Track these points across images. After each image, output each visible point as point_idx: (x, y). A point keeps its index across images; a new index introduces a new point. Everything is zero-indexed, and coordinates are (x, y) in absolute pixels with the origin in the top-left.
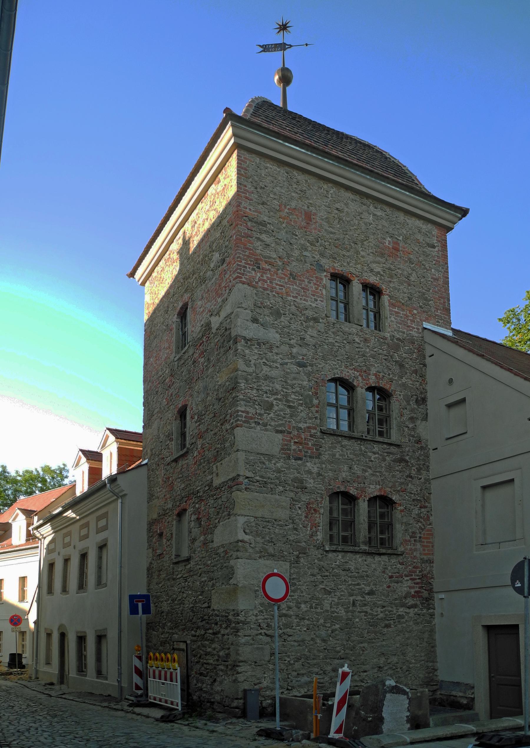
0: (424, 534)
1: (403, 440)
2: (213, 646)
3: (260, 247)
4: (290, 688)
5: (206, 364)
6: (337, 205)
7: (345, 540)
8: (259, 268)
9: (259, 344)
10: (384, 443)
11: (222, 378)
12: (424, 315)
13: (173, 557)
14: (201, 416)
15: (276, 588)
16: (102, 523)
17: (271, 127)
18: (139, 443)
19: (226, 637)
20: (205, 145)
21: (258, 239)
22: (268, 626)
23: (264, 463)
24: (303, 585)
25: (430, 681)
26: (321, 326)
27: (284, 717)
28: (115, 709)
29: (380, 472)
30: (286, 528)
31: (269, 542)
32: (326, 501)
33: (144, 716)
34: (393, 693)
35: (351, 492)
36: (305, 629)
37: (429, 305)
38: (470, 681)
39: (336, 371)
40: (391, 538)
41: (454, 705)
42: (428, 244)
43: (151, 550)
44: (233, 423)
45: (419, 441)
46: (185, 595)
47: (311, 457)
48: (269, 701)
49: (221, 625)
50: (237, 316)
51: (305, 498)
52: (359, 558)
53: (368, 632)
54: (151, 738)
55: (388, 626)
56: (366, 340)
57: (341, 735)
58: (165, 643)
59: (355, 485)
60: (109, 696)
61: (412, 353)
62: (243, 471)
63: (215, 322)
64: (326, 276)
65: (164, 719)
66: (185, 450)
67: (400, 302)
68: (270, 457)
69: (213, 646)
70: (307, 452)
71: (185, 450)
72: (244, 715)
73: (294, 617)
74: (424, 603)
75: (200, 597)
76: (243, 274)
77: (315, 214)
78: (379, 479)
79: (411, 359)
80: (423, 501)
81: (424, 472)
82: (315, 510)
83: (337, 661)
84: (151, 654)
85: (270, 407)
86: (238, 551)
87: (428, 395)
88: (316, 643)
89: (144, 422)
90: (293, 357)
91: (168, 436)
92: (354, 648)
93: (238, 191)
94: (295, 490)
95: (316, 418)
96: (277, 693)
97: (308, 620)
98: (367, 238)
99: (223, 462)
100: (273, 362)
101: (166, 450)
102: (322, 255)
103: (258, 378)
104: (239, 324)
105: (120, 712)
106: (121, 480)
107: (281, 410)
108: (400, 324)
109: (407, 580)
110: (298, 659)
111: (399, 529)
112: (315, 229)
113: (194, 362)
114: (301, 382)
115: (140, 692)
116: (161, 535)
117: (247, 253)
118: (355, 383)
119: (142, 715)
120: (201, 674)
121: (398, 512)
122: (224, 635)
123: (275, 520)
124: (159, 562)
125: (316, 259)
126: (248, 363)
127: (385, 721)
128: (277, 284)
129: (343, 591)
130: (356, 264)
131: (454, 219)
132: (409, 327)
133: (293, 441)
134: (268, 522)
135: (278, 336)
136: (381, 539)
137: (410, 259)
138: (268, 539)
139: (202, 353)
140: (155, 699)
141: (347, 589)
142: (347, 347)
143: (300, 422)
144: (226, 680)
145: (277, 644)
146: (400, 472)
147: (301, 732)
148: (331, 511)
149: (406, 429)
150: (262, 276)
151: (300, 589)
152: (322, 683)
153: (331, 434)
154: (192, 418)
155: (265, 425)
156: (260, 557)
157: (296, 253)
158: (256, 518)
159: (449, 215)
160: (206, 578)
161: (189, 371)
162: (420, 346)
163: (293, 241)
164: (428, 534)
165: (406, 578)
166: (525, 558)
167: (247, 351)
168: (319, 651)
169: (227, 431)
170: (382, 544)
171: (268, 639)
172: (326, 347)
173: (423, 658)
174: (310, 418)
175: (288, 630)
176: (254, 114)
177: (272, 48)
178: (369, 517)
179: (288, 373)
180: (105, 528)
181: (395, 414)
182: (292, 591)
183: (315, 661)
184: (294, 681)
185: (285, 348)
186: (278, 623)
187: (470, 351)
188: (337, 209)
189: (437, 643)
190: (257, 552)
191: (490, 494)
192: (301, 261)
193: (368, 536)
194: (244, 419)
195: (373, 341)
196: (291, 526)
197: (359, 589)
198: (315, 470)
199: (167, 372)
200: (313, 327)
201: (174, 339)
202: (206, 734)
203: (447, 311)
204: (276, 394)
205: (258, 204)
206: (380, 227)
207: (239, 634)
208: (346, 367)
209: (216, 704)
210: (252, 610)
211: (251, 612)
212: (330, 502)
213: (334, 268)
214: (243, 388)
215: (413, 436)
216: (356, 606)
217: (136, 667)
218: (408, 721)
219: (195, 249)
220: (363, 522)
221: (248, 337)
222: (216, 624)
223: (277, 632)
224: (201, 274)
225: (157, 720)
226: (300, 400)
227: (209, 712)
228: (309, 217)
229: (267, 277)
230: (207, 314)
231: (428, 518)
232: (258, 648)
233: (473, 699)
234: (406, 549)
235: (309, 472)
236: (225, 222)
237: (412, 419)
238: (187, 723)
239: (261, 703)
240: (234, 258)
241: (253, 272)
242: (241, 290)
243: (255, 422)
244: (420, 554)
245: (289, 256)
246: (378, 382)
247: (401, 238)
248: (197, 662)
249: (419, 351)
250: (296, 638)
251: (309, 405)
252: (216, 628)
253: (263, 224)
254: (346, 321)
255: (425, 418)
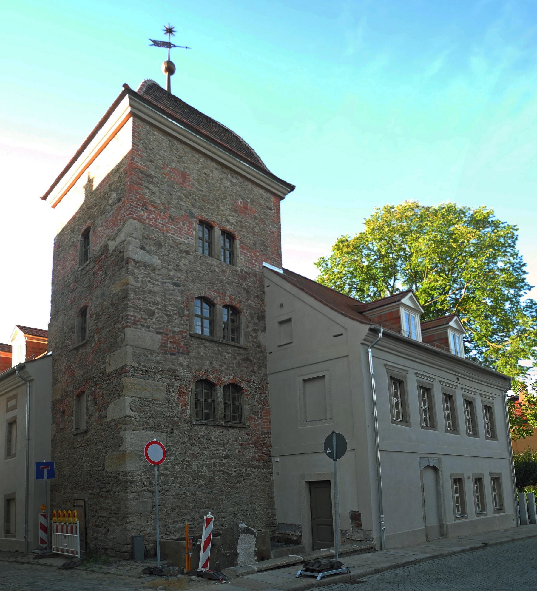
0: (264, 413)
1: (248, 345)
2: (107, 502)
3: (148, 194)
4: (168, 533)
5: (103, 276)
6: (205, 171)
7: (207, 416)
8: (146, 209)
9: (145, 266)
10: (235, 346)
11: (116, 289)
12: (264, 257)
13: (74, 430)
14: (98, 316)
15: (156, 453)
16: (12, 403)
17: (159, 105)
18: (45, 339)
19: (117, 493)
20: (107, 108)
21: (147, 187)
22: (151, 483)
23: (147, 356)
24: (176, 451)
25: (271, 524)
26: (191, 258)
27: (164, 557)
28: (21, 563)
29: (232, 367)
30: (163, 406)
31: (150, 417)
32: (193, 387)
33: (48, 566)
34: (245, 533)
35: (211, 380)
36: (179, 485)
37: (267, 250)
38: (298, 523)
39: (201, 291)
40: (241, 415)
41: (288, 541)
42: (267, 207)
43: (55, 425)
44: (123, 324)
45: (259, 346)
46: (83, 461)
47: (182, 354)
48: (152, 545)
49: (113, 484)
50: (129, 243)
51: (177, 384)
52: (218, 430)
53: (225, 487)
54: (54, 584)
55: (239, 482)
56: (223, 271)
57: (207, 568)
58: (66, 502)
59: (214, 375)
60: (17, 551)
61: (255, 283)
62: (130, 362)
63: (112, 245)
64: (195, 221)
65: (66, 567)
66: (85, 341)
67: (248, 246)
68: (152, 352)
69: (107, 502)
70: (179, 350)
71: (85, 341)
72: (132, 557)
73: (170, 476)
74: (265, 465)
75: (96, 462)
76: (134, 212)
77: (189, 175)
78: (231, 372)
79: (254, 287)
80: (263, 388)
81: (263, 369)
82: (184, 393)
83: (203, 510)
84: (55, 512)
85: (152, 314)
86: (126, 424)
87: (266, 314)
88: (187, 496)
89: (51, 316)
90: (170, 278)
91: (71, 329)
92: (215, 499)
93: (132, 149)
94: (170, 377)
95: (187, 325)
96: (158, 538)
97: (181, 478)
98: (225, 197)
99: (115, 353)
100: (156, 280)
101: (69, 340)
102: (193, 205)
103: (143, 291)
104: (130, 249)
105: (25, 565)
106: (28, 368)
107: (161, 317)
108: (247, 262)
109: (252, 447)
110: (173, 510)
111: (246, 408)
112: (189, 186)
113: (94, 274)
114: (176, 298)
115: (44, 545)
116: (63, 412)
117: (138, 197)
118: (215, 302)
119: (46, 565)
120: (97, 526)
121: (245, 396)
122: (115, 492)
123: (155, 400)
124: (62, 434)
125: (189, 208)
126: (136, 279)
127: (239, 555)
128: (160, 223)
129: (206, 455)
130: (217, 215)
131: (285, 192)
132: (253, 264)
133: (169, 341)
134: (149, 401)
135: (159, 261)
136: (234, 416)
137: (255, 216)
138: (149, 414)
139: (101, 267)
140: (58, 550)
141: (209, 454)
142: (210, 275)
143: (175, 327)
144: (117, 529)
145: (157, 498)
146: (247, 368)
147: (177, 568)
148: (197, 395)
149: (251, 337)
150: (149, 215)
151: (174, 454)
152: (192, 528)
153: (197, 338)
154: (91, 316)
155: (148, 327)
156: (143, 429)
157: (175, 202)
158: (140, 398)
159: (282, 188)
160: (100, 447)
161: (90, 280)
162: (261, 278)
163: (172, 192)
164: (266, 413)
165: (252, 446)
166: (333, 432)
167: (136, 271)
168: (189, 502)
169: (119, 329)
170: (234, 420)
171: (150, 494)
172: (194, 273)
173: (265, 506)
174: (182, 325)
175: (166, 486)
176: (146, 92)
177: (161, 44)
178: (225, 399)
179: (166, 290)
180: (15, 407)
181: (243, 326)
182: (168, 456)
183: (187, 511)
184: (171, 528)
185: (164, 271)
186: (158, 481)
187: (295, 285)
188: (205, 174)
189: (275, 495)
190: (141, 425)
191: (309, 386)
192: (178, 208)
193: (224, 414)
194: (132, 322)
195: (228, 272)
196: (167, 405)
197: (218, 454)
198: (185, 363)
199: (72, 278)
200: (185, 258)
201: (78, 254)
202: (101, 576)
203: (280, 255)
204: (157, 304)
205: (147, 161)
206: (235, 191)
207: (127, 491)
208: (209, 289)
209: (109, 550)
210: (137, 471)
211: (137, 473)
212: (196, 388)
213: (202, 216)
214: (132, 298)
215: (256, 343)
216: (216, 467)
217: (41, 524)
218: (255, 555)
219: (98, 187)
220: (222, 403)
221: (137, 260)
222: (109, 483)
223: (157, 488)
224: (102, 207)
225: (59, 568)
226: (175, 310)
227: (104, 558)
228: (184, 176)
229: (153, 217)
230: (105, 238)
231: (267, 401)
232: (142, 502)
233: (301, 536)
234: (251, 424)
235: (181, 365)
236: (121, 170)
237: (255, 330)
238: (85, 568)
239: (145, 547)
240: (128, 199)
241: (142, 212)
242: (132, 225)
243: (141, 325)
244: (261, 427)
245: (169, 203)
246: (232, 302)
247: (249, 201)
248: (93, 516)
249: (260, 282)
250: (172, 492)
251: (181, 314)
252: (109, 487)
253: (150, 176)
254: (209, 255)
255: (264, 330)
